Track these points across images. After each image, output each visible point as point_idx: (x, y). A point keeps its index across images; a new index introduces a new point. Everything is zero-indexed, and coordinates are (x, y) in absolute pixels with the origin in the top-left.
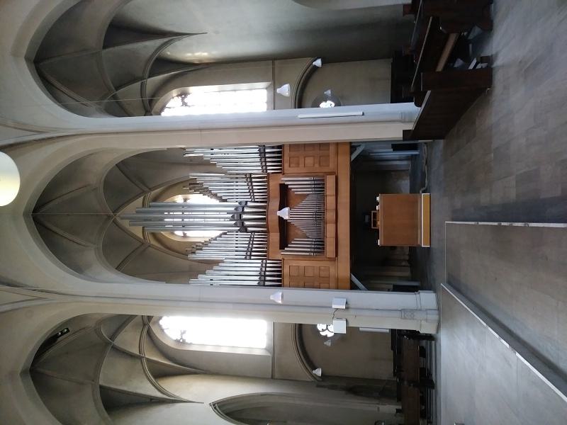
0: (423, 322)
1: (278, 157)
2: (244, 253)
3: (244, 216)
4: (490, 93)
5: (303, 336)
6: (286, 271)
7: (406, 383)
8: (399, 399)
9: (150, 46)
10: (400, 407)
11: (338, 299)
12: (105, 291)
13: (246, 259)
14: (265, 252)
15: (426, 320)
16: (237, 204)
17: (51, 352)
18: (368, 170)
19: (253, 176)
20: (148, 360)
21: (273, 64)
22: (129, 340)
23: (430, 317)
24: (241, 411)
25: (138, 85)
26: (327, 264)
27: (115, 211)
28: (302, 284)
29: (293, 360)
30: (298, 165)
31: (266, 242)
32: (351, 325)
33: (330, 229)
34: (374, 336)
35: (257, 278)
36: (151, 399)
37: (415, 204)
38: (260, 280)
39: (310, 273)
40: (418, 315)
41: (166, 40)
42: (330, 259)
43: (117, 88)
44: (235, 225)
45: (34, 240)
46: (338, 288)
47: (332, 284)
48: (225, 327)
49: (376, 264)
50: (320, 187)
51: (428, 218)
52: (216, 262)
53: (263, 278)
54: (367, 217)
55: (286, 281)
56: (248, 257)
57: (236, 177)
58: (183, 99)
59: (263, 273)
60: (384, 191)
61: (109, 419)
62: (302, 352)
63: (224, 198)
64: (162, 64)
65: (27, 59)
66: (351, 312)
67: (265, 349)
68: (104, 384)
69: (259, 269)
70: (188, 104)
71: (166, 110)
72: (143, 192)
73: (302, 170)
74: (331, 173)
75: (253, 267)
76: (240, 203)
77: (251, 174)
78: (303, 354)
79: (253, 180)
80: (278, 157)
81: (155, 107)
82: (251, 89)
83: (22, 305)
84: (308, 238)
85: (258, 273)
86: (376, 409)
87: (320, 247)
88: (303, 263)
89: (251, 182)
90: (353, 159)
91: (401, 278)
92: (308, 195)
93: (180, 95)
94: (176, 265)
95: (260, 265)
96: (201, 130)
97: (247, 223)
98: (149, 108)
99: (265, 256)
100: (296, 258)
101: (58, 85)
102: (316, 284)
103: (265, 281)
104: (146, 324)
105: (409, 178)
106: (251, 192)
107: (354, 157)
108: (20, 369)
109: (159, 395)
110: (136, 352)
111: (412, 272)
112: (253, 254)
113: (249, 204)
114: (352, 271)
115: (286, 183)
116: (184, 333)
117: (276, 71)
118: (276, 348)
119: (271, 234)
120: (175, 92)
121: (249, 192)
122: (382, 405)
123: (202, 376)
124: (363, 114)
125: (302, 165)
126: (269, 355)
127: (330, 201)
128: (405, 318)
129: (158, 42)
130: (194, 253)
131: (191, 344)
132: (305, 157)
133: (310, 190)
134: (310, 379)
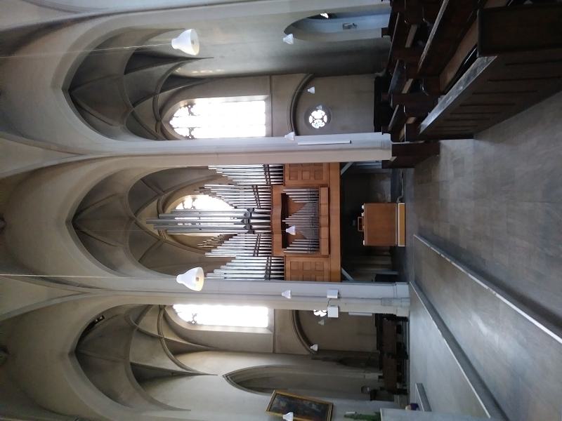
0: (399, 308)
1: (279, 175)
2: (253, 252)
3: (252, 221)
4: (438, 159)
5: (300, 320)
6: (288, 265)
7: (385, 355)
8: (381, 368)
9: (163, 69)
10: (381, 374)
11: (331, 291)
12: (131, 285)
15: (401, 306)
16: (246, 210)
17: (91, 335)
18: (357, 181)
19: (259, 187)
20: (165, 339)
21: (270, 78)
22: (150, 324)
23: (404, 304)
24: (248, 381)
25: (150, 100)
26: (322, 260)
27: (136, 214)
28: (301, 276)
29: (291, 337)
30: (296, 178)
31: (270, 242)
32: (341, 311)
33: (324, 232)
34: (361, 319)
35: (264, 272)
36: (173, 373)
37: (394, 211)
38: (266, 273)
39: (307, 268)
40: (395, 303)
41: (177, 63)
42: (327, 257)
43: (134, 105)
44: (245, 228)
45: (76, 244)
46: (330, 280)
47: (326, 277)
48: (229, 308)
49: (362, 258)
50: (315, 197)
51: (401, 224)
52: (229, 260)
53: (268, 272)
54: (354, 222)
55: (288, 274)
56: (256, 255)
57: (245, 187)
58: (189, 109)
59: (268, 268)
60: (367, 201)
61: (142, 390)
62: (302, 337)
64: (174, 80)
65: (64, 90)
66: (342, 300)
67: (267, 328)
68: (134, 362)
69: (265, 265)
70: (195, 114)
72: (159, 195)
73: (299, 182)
74: (323, 186)
75: (260, 263)
76: (248, 209)
77: (257, 185)
78: (301, 334)
79: (259, 190)
80: (279, 175)
81: (165, 117)
82: (251, 101)
83: (65, 299)
84: (306, 239)
85: (264, 268)
87: (316, 246)
88: (301, 260)
89: (258, 192)
90: (342, 173)
91: (383, 266)
92: (305, 203)
94: (176, 252)
95: (266, 261)
96: (217, 154)
97: (254, 227)
98: (158, 116)
99: (269, 254)
100: (295, 257)
101: (88, 108)
102: (313, 276)
103: (270, 274)
104: (163, 313)
105: (390, 179)
106: (257, 200)
107: (342, 172)
108: (68, 350)
109: (179, 369)
110: (155, 333)
111: (392, 260)
112: (260, 252)
114: (343, 265)
115: (287, 194)
116: (191, 129)
117: (273, 85)
118: (276, 327)
119: (275, 235)
120: (182, 103)
121: (256, 200)
122: (369, 373)
123: (217, 353)
124: (351, 142)
125: (300, 178)
127: (324, 208)
128: (384, 305)
129: (171, 65)
130: (210, 252)
131: (201, 325)
132: (302, 171)
134: (306, 353)
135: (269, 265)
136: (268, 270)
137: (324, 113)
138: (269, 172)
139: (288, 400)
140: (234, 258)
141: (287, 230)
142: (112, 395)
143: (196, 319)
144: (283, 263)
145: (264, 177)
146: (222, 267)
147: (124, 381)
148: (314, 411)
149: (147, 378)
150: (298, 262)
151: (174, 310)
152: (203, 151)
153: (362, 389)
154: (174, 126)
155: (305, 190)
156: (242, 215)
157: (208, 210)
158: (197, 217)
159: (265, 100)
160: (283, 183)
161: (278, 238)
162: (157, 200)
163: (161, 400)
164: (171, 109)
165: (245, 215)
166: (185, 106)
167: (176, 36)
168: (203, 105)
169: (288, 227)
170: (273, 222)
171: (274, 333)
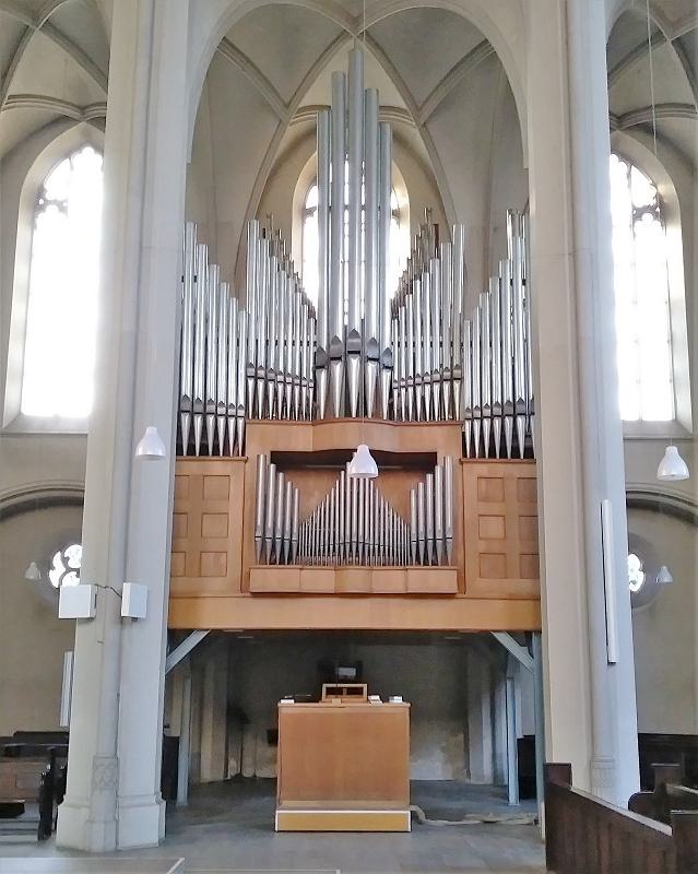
0: (85, 811)
2: (261, 362)
3: (355, 362)
6: (217, 466)
11: (143, 598)
15: (91, 821)
18: (467, 674)
19: (456, 385)
26: (234, 572)
27: (369, 36)
28: (184, 507)
32: (78, 629)
33: (322, 579)
42: (245, 579)
44: (333, 340)
47: (183, 584)
52: (239, 291)
55: (193, 467)
56: (252, 371)
57: (456, 344)
59: (272, 375)
60: (414, 715)
66: (112, 631)
67: (20, 413)
69: (222, 398)
70: (638, 223)
73: (472, 508)
74: (462, 581)
75: (230, 388)
76: (389, 352)
77: (461, 379)
79: (446, 386)
82: (673, 380)
85: (211, 395)
87: (280, 554)
88: (235, 509)
89: (441, 381)
92: (409, 525)
96: (574, 254)
97: (338, 368)
98: (629, 123)
99: (255, 412)
100: (247, 490)
102: (184, 544)
103: (192, 414)
104: (85, 116)
106: (416, 381)
113: (386, 375)
114: (215, 636)
115: (438, 470)
116: (62, 207)
120: (667, 189)
125: (483, 508)
128: (95, 767)
131: (33, 225)
135: (280, 378)
138: (492, 417)
140: (242, 306)
143: (51, 210)
144: (226, 452)
145: (487, 400)
152: (582, 209)
157: (349, 260)
158: (368, 199)
159: (676, 421)
160: (468, 454)
162: (403, 105)
165: (374, 342)
166: (659, 197)
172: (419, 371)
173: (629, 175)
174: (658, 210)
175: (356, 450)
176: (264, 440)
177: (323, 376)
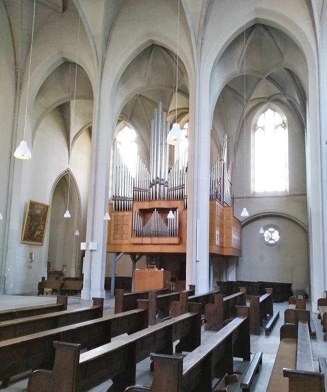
1: (118, 208)
3: (158, 185)
6: (126, 213)
13: (134, 188)
14: (156, 198)
16: (167, 180)
35: (128, 196)
56: (135, 189)
58: (281, 125)
63: (171, 171)
65: (256, 19)
71: (273, 112)
76: (167, 182)
78: (250, 220)
80: (118, 208)
81: (272, 104)
84: (143, 227)
86: (72, 266)
87: (139, 235)
93: (284, 123)
99: (134, 199)
100: (132, 219)
103: (121, 200)
106: (174, 189)
108: (66, 57)
109: (72, 136)
112: (137, 192)
113: (166, 188)
116: (263, 128)
117: (297, 197)
120: (285, 118)
126: (251, 193)
133: (175, 227)
136: (124, 199)
137: (276, 240)
139: (43, 215)
141: (171, 212)
142: (42, 91)
143: (259, 130)
146: (141, 160)
147: (54, 98)
148: (34, 232)
149: (62, 112)
150: (129, 221)
151: (124, 127)
153: (65, 266)
154: (266, 113)
155: (177, 228)
156: (163, 178)
159: (286, 191)
161: (146, 205)
163: (40, 127)
164: (280, 110)
166: (283, 121)
167: (28, 146)
168: (284, 135)
169: (173, 212)
170: (156, 202)
171: (251, 198)
172: (181, 184)
173: (274, 115)
174: (283, 125)
175: (177, 208)
176: (137, 207)
177: (151, 189)
